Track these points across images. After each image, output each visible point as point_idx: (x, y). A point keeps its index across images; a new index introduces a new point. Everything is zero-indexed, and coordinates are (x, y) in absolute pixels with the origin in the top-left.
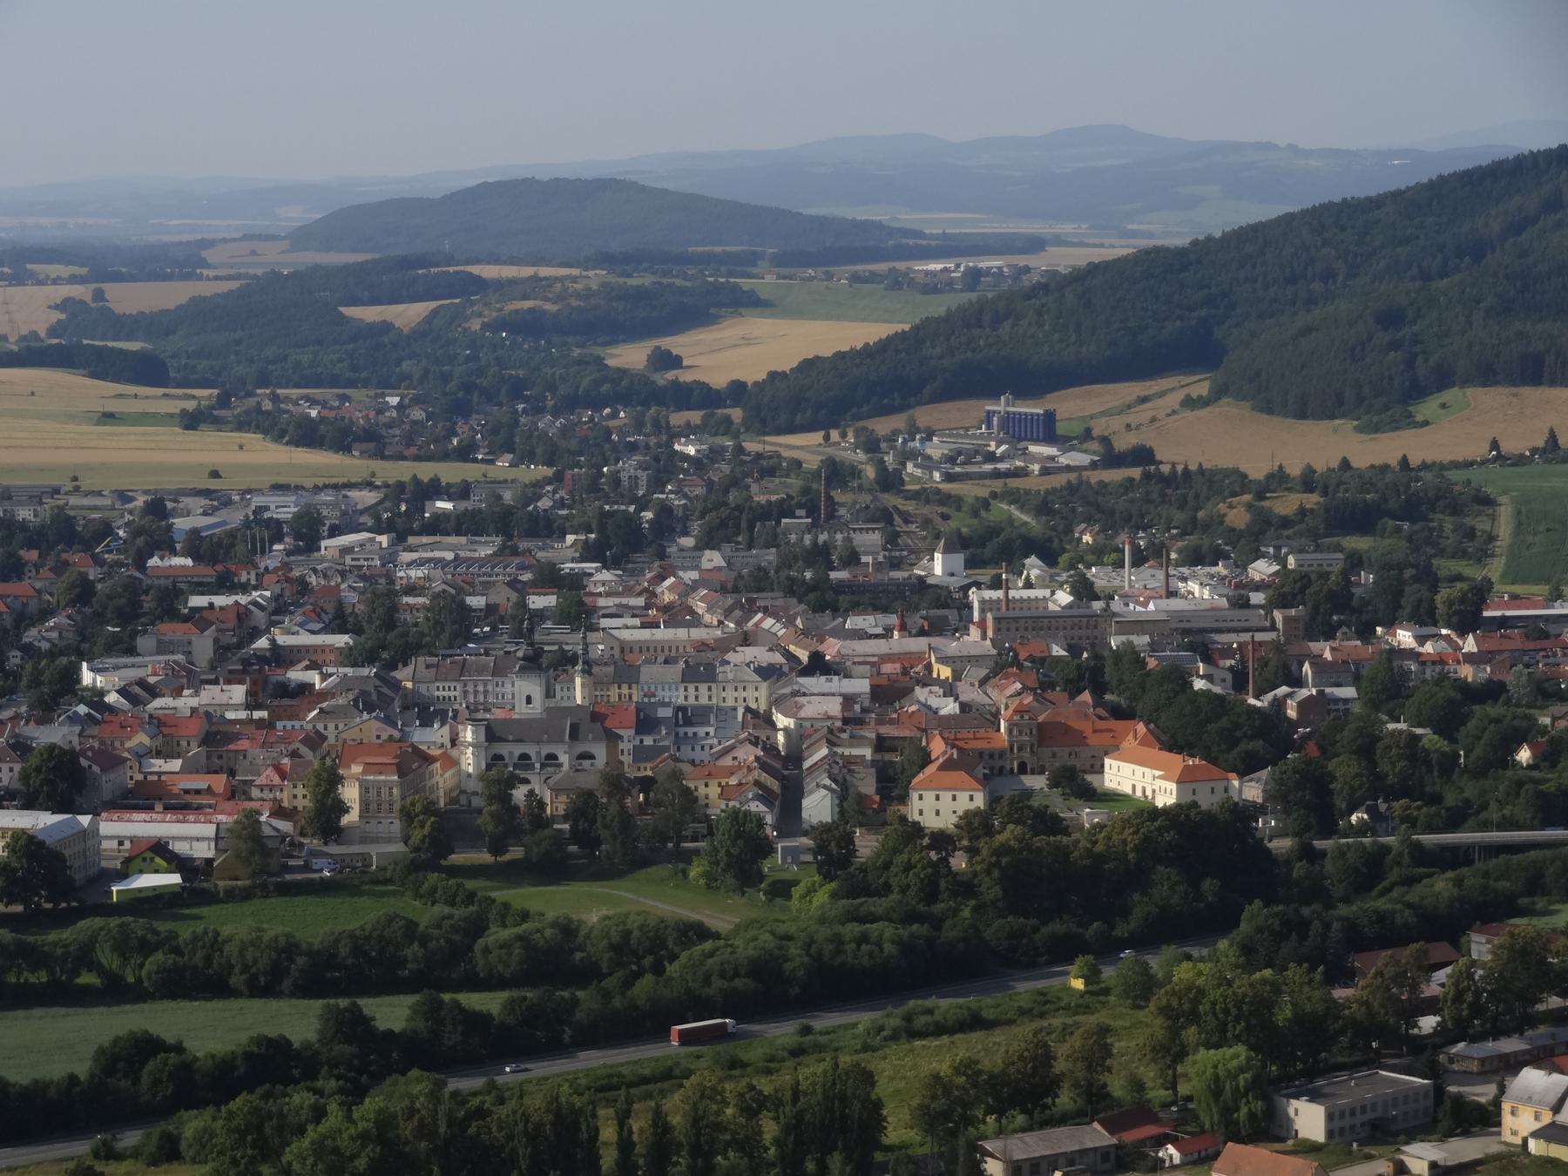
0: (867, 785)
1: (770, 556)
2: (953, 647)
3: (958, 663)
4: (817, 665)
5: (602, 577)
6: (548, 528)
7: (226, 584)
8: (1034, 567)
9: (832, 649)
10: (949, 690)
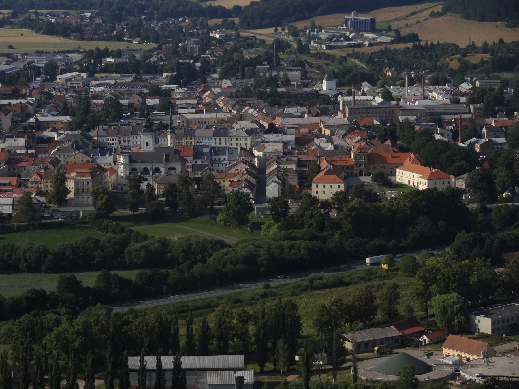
0: (294, 181)
1: (251, 82)
2: (331, 121)
3: (333, 128)
4: (272, 129)
5: (179, 91)
6: (155, 70)
7: (16, 95)
8: (366, 86)
9: (278, 122)
10: (329, 139)
